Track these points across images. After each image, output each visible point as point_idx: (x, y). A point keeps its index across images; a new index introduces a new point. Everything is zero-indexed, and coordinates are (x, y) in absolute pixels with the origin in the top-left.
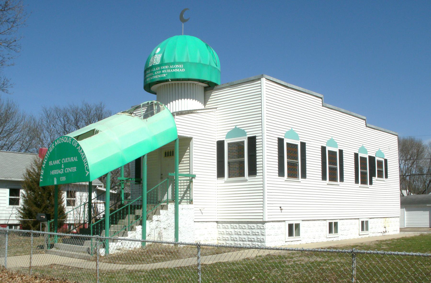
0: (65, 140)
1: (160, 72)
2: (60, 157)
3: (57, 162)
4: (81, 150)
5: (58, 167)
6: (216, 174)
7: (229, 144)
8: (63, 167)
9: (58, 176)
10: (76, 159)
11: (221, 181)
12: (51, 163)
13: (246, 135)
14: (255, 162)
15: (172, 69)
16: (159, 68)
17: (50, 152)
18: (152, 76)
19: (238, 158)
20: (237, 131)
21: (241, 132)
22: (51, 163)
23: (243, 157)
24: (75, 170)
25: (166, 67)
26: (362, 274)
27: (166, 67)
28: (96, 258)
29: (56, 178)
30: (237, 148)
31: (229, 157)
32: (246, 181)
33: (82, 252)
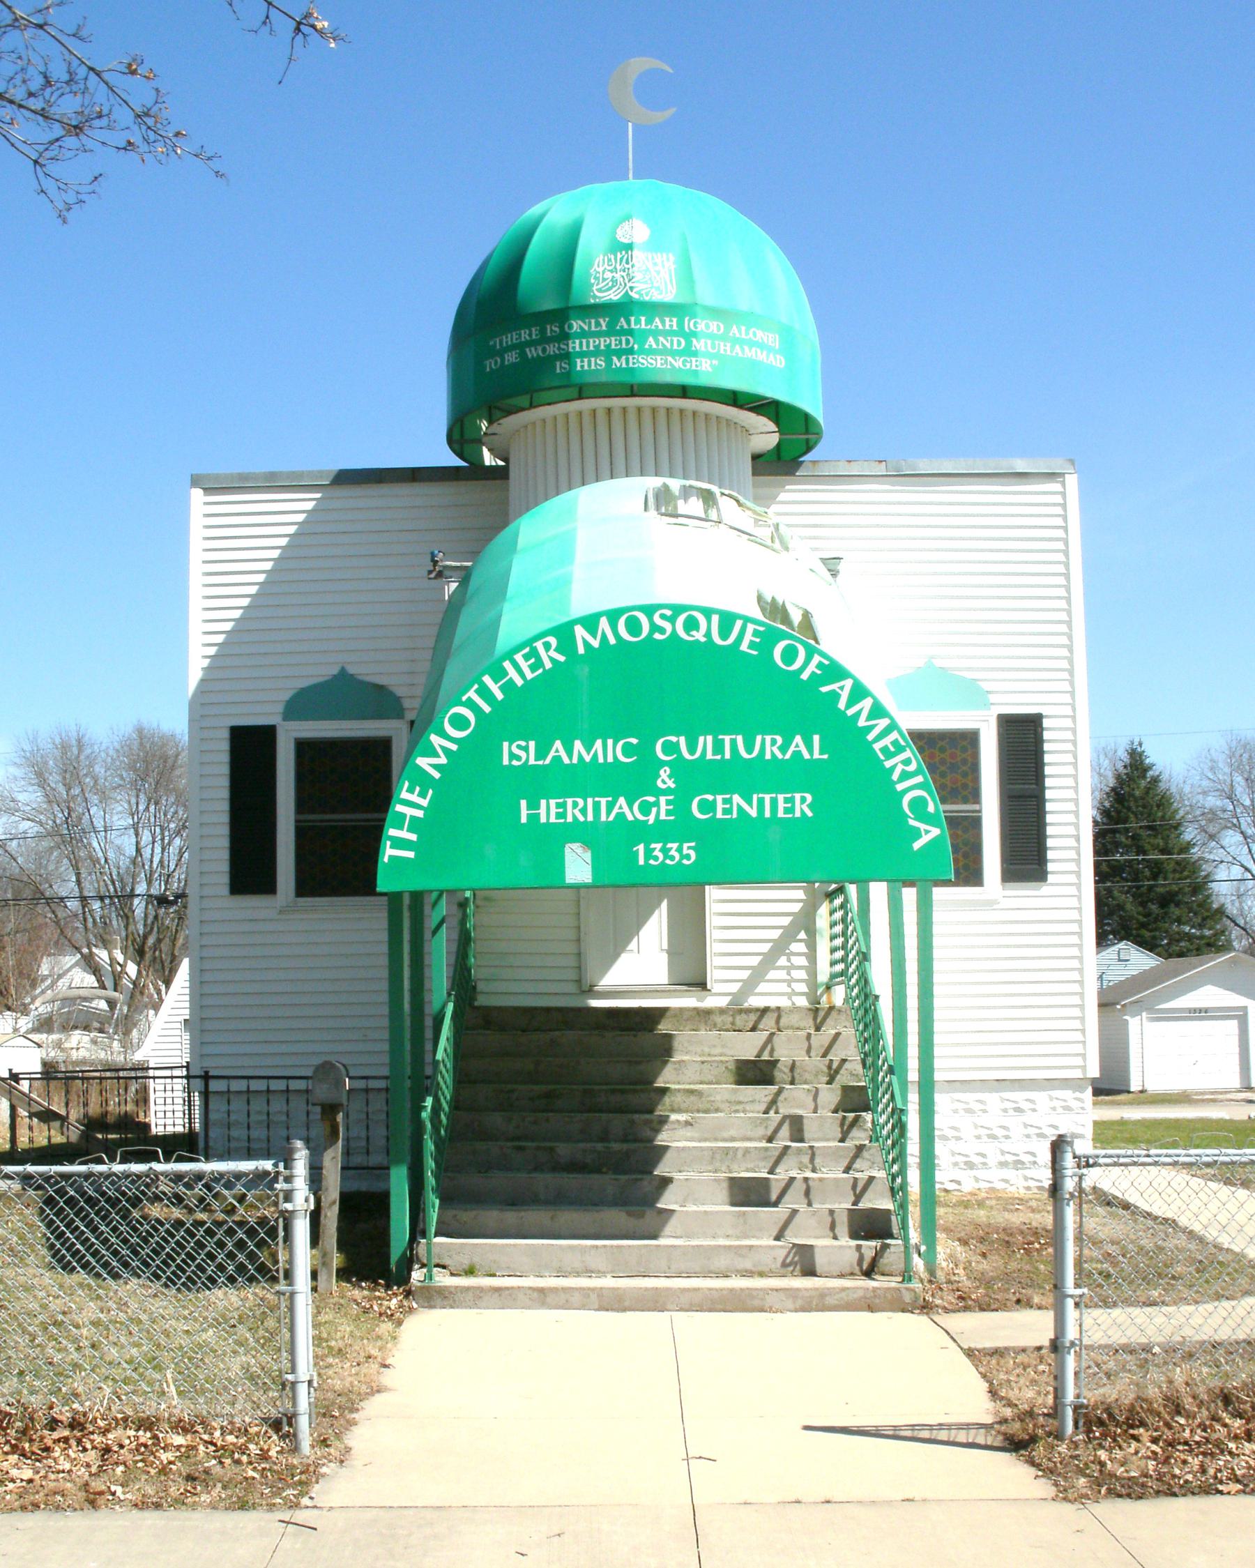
1: (677, 343)
6: (226, 879)
7: (304, 748)
10: (809, 749)
15: (741, 342)
16: (671, 323)
18: (630, 351)
25: (525, 335)
26: (261, 1244)
27: (525, 335)
28: (1172, 1419)
31: (302, 804)
32: (990, 904)
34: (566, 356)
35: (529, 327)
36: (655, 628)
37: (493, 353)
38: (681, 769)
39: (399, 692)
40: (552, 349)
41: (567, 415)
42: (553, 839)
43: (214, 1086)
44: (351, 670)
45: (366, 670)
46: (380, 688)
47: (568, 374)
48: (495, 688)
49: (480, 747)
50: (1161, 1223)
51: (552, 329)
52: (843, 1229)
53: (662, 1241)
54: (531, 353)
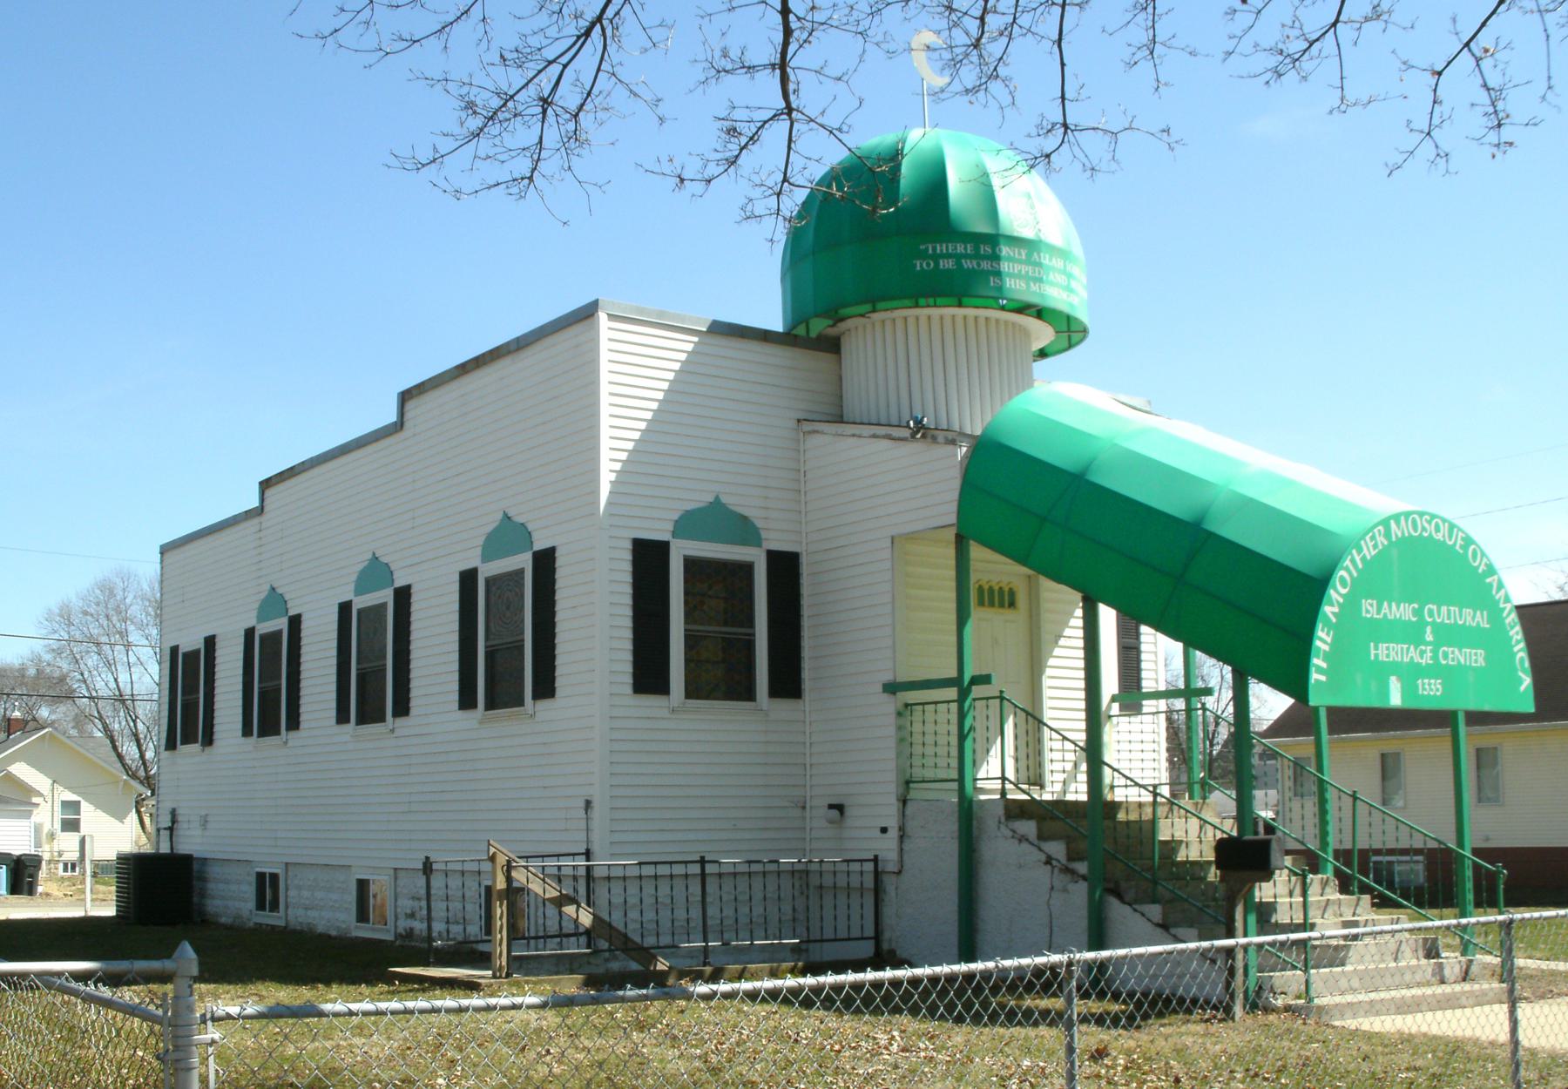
0: (1437, 529)
2: (1414, 592)
3: (1403, 612)
4: (1502, 593)
5: (1411, 633)
6: (629, 679)
7: (691, 564)
8: (1429, 637)
9: (1409, 674)
10: (1480, 620)
11: (651, 704)
12: (1368, 608)
13: (760, 546)
14: (1138, 670)
17: (1363, 559)
19: (726, 624)
20: (716, 518)
21: (745, 530)
22: (1368, 608)
23: (750, 621)
24: (1480, 659)
25: (960, 249)
27: (960, 249)
29: (1399, 679)
30: (719, 584)
33: (1419, 985)
34: (998, 274)
35: (965, 243)
36: (1424, 529)
37: (923, 256)
38: (1437, 628)
39: (759, 524)
40: (985, 265)
41: (942, 318)
42: (1384, 671)
43: (710, 869)
44: (724, 499)
45: (736, 502)
46: (745, 518)
47: (1000, 288)
48: (1357, 559)
49: (1351, 603)
50: (764, 1000)
51: (985, 249)
52: (1421, 953)
53: (1349, 968)
54: (967, 264)
